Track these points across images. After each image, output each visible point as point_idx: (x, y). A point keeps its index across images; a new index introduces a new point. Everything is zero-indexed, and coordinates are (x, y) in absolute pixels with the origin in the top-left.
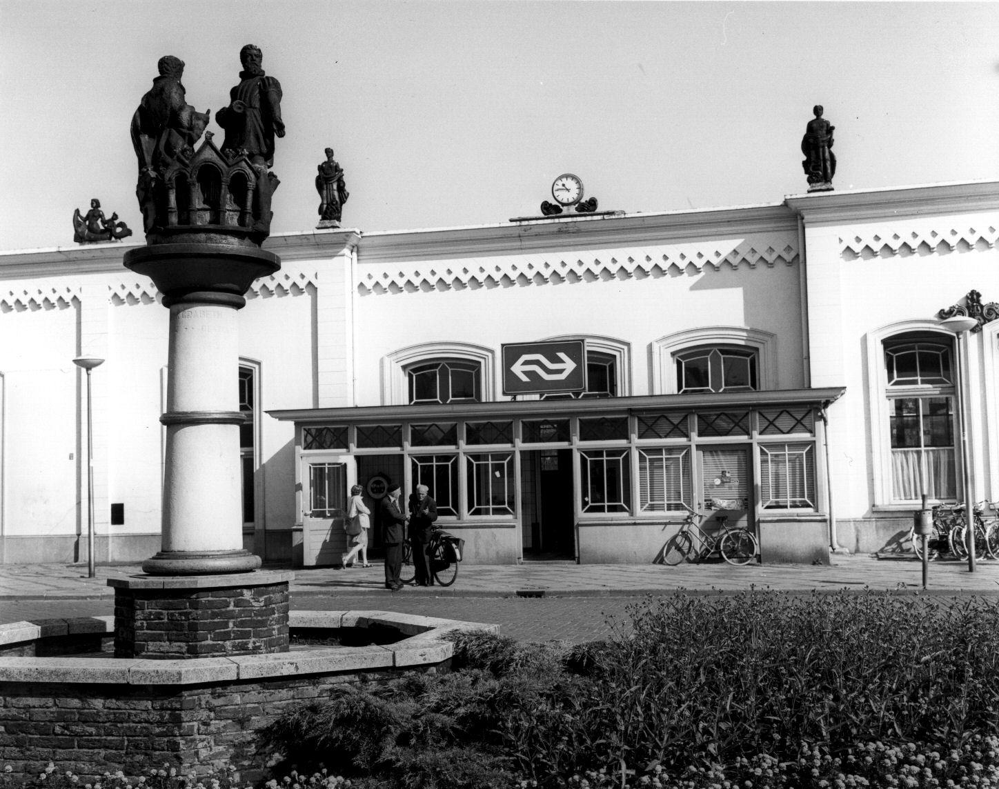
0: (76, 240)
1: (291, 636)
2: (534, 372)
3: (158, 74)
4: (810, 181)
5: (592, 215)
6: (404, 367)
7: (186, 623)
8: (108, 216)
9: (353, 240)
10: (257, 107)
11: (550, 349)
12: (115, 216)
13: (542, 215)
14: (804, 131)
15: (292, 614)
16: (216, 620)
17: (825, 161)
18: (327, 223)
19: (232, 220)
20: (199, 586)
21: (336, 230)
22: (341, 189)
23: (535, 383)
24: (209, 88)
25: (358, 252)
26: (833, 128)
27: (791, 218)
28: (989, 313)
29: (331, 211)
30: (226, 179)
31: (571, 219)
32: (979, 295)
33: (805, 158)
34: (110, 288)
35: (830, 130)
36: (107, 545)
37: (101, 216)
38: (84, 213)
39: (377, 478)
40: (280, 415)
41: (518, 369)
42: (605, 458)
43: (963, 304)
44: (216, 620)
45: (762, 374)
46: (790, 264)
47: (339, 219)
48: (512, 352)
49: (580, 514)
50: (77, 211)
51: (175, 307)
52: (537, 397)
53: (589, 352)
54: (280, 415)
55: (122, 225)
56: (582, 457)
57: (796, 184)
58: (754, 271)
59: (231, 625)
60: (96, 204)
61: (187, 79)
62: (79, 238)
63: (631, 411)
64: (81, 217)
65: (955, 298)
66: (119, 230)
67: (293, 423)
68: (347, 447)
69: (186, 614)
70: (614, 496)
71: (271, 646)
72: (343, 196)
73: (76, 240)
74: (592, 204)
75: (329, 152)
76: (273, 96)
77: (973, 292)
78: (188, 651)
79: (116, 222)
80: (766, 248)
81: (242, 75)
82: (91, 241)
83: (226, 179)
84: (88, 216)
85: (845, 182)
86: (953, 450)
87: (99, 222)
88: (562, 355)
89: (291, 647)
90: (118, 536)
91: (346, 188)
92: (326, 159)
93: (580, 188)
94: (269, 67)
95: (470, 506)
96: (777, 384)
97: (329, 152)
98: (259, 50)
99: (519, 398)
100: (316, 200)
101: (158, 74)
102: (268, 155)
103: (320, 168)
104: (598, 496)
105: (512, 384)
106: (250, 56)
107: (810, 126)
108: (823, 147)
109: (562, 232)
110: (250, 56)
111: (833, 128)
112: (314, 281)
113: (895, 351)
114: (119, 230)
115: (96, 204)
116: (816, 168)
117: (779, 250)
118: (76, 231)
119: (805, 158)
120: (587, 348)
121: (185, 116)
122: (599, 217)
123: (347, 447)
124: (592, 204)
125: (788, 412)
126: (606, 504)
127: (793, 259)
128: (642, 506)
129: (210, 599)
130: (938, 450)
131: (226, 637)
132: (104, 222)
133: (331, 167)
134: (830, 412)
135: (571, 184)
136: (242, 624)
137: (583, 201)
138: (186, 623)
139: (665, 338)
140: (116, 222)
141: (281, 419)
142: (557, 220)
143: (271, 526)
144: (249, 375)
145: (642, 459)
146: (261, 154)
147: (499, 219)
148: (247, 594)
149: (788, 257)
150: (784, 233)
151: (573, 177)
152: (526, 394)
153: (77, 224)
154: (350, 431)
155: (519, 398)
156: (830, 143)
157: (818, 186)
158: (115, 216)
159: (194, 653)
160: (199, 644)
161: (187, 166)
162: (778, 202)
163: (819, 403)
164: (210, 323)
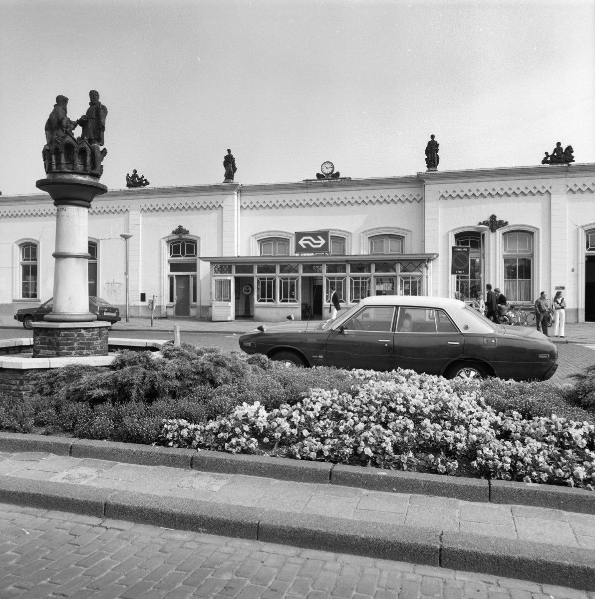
0: (127, 186)
1: (109, 349)
2: (308, 244)
3: (56, 103)
4: (428, 167)
5: (323, 180)
6: (259, 241)
7: (55, 343)
8: (140, 177)
9: (238, 188)
10: (96, 117)
11: (315, 235)
12: (143, 177)
13: (316, 178)
14: (426, 146)
15: (110, 339)
16: (68, 342)
17: (434, 158)
18: (228, 181)
19: (79, 167)
20: (60, 327)
21: (231, 184)
22: (234, 166)
23: (309, 249)
24: (77, 110)
25: (241, 192)
26: (439, 144)
27: (419, 181)
28: (499, 225)
29: (229, 176)
30: (77, 150)
31: (329, 179)
32: (495, 217)
33: (426, 157)
34: (439, 192)
35: (437, 145)
36: (139, 310)
37: (137, 176)
38: (131, 176)
39: (247, 286)
40: (205, 259)
41: (301, 242)
42: (336, 280)
43: (489, 220)
44: (68, 342)
45: (406, 247)
46: (419, 202)
47: (233, 179)
48: (299, 235)
49: (256, 302)
50: (128, 175)
51: (61, 207)
52: (313, 254)
53: (331, 236)
54: (205, 259)
55: (145, 180)
56: (280, 280)
57: (423, 168)
58: (397, 205)
59: (75, 344)
60: (135, 171)
61: (69, 106)
62: (128, 186)
63: (347, 261)
64: (130, 177)
65: (486, 218)
66: (144, 182)
67: (209, 263)
68: (230, 272)
69: (55, 339)
70: (269, 296)
71: (97, 353)
72: (235, 169)
73: (127, 186)
74: (338, 174)
75: (229, 151)
76: (102, 113)
77: (493, 215)
78: (56, 354)
79: (143, 179)
80: (394, 195)
81: (90, 104)
82: (133, 186)
83: (77, 150)
84: (132, 176)
85: (441, 168)
86: (530, 281)
87: (136, 179)
88: (320, 237)
89: (109, 353)
90: (143, 306)
91: (236, 166)
92: (228, 154)
93: (333, 168)
94: (102, 100)
95: (281, 298)
96: (411, 252)
97: (229, 151)
98: (98, 93)
99: (302, 255)
100: (224, 171)
101: (56, 103)
102: (101, 140)
103: (225, 157)
104: (263, 296)
105: (299, 249)
106: (94, 95)
107: (429, 143)
108: (434, 153)
109: (325, 185)
110: (94, 95)
111: (439, 144)
112: (549, 190)
113: (460, 239)
114: (144, 182)
115: (135, 171)
116: (431, 161)
117: (414, 196)
118: (127, 182)
119: (426, 157)
120: (330, 235)
121: (64, 122)
122: (340, 180)
123: (230, 272)
124: (338, 174)
125: (412, 263)
126: (266, 299)
127: (420, 200)
128: (351, 300)
129: (65, 332)
130: (509, 281)
131: (73, 349)
132: (138, 179)
133: (229, 157)
134: (430, 265)
135: (329, 166)
136: (81, 344)
137: (334, 173)
138: (55, 343)
139: (366, 231)
140: (143, 179)
141: (204, 261)
142: (322, 181)
143: (203, 304)
144: (195, 243)
145: (401, 281)
146: (95, 139)
147: (299, 179)
148: (83, 331)
149: (418, 199)
150: (414, 189)
151: (330, 163)
152: (308, 253)
153: (128, 180)
154: (254, 266)
155: (302, 255)
156: (437, 151)
157: (432, 169)
158: (143, 177)
159: (58, 355)
160: (60, 352)
161: (59, 143)
162: (415, 174)
163: (425, 260)
164: (76, 215)
